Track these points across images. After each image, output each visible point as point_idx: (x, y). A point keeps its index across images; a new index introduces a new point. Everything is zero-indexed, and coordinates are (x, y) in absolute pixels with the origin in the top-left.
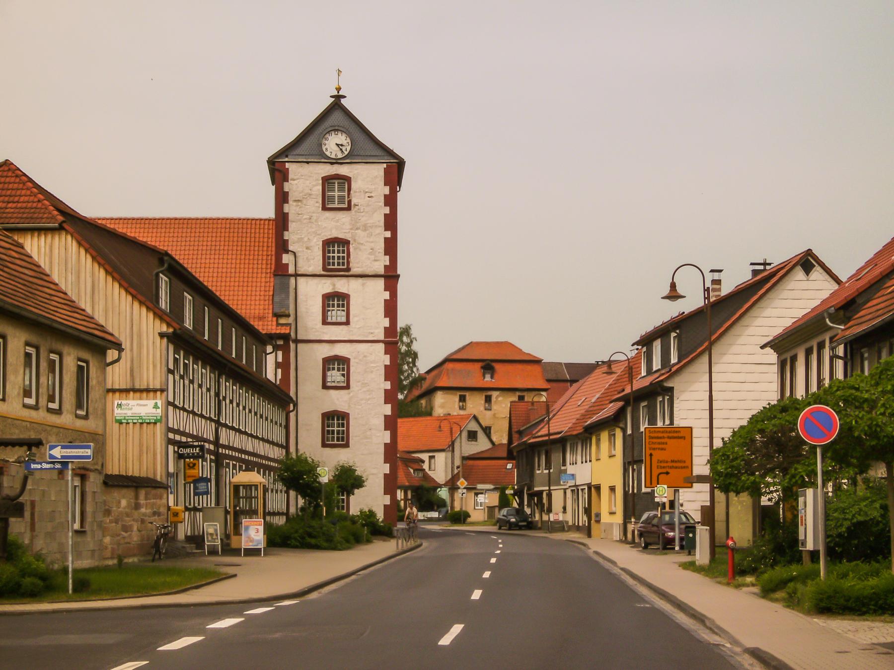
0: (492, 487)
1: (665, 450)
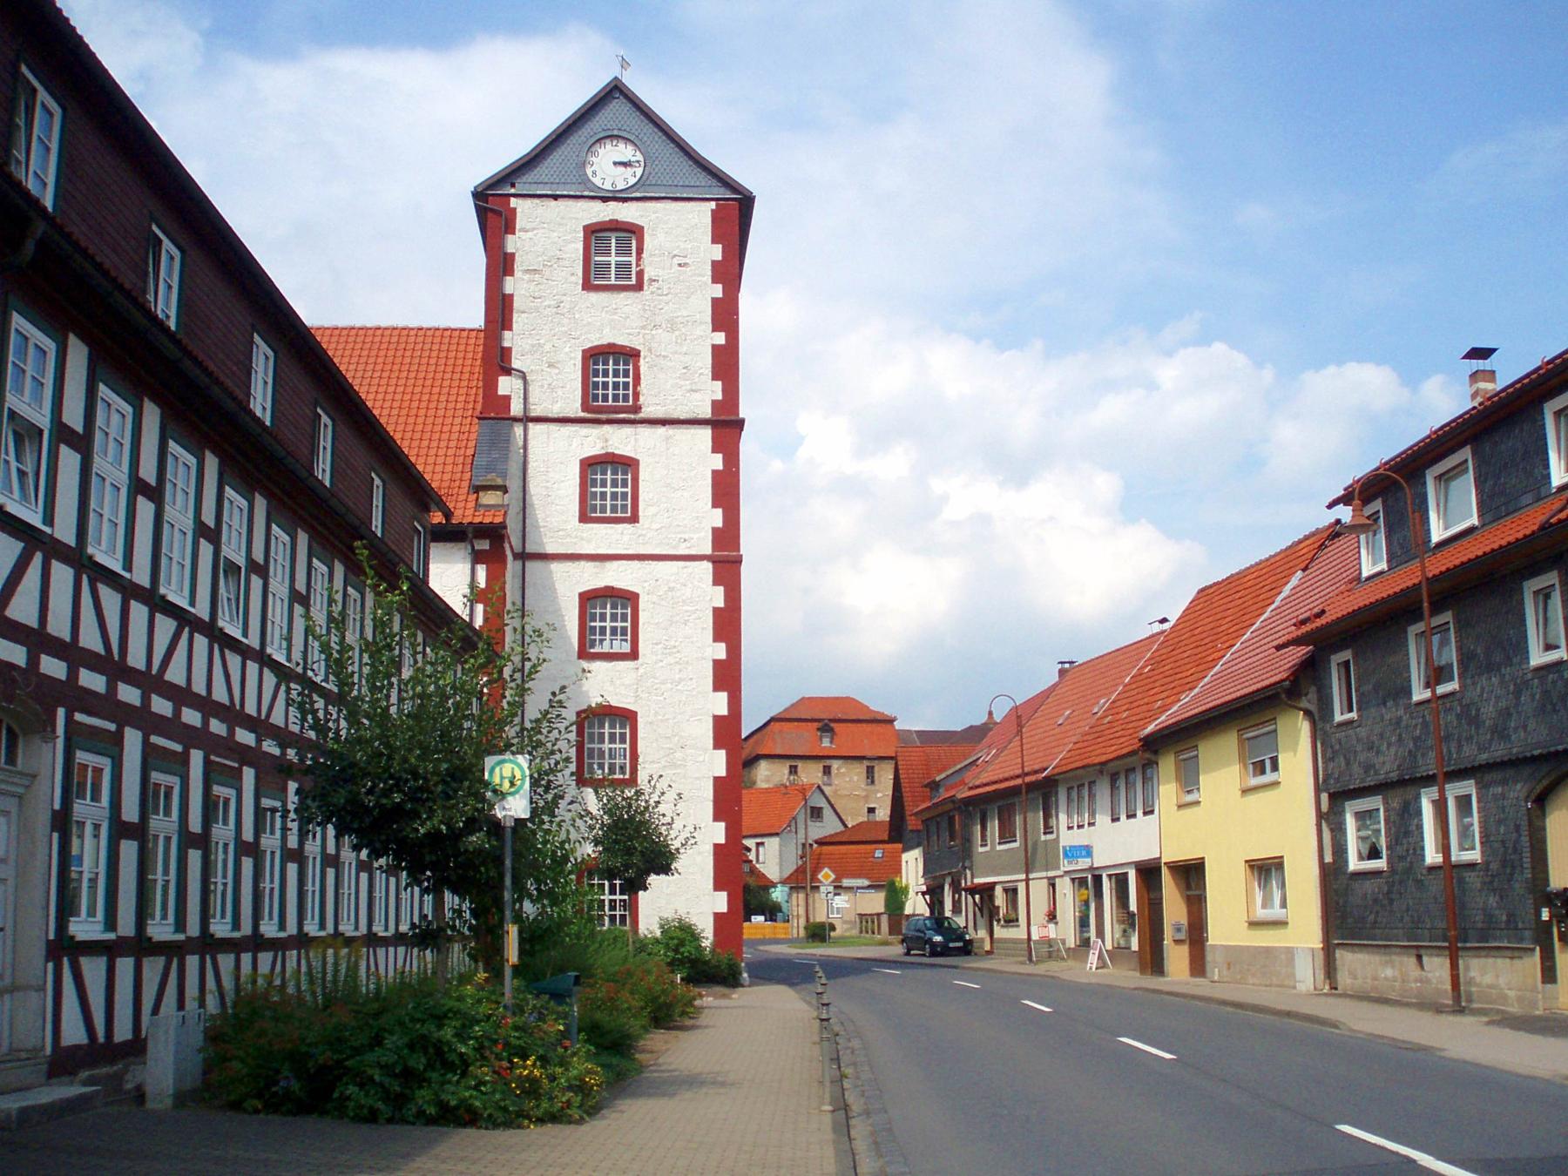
0: (866, 883)
1: (1198, 803)
